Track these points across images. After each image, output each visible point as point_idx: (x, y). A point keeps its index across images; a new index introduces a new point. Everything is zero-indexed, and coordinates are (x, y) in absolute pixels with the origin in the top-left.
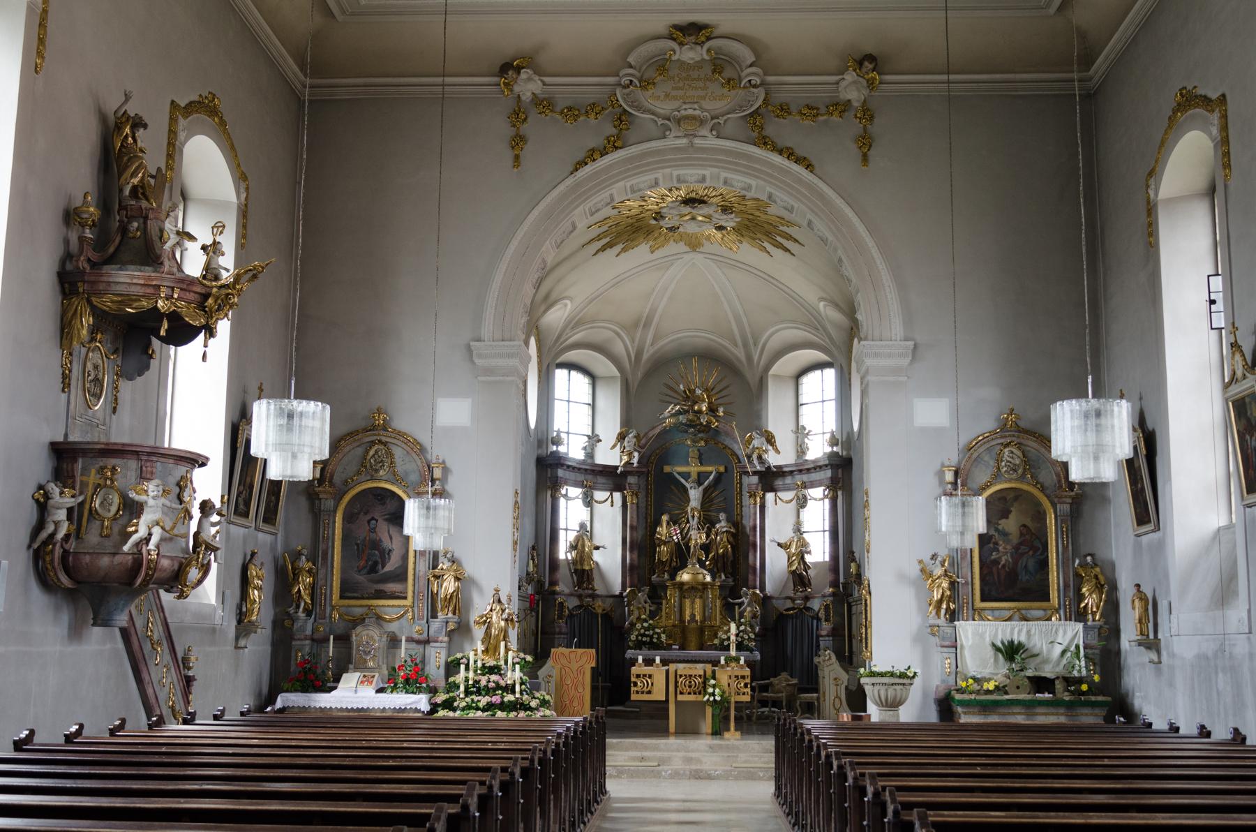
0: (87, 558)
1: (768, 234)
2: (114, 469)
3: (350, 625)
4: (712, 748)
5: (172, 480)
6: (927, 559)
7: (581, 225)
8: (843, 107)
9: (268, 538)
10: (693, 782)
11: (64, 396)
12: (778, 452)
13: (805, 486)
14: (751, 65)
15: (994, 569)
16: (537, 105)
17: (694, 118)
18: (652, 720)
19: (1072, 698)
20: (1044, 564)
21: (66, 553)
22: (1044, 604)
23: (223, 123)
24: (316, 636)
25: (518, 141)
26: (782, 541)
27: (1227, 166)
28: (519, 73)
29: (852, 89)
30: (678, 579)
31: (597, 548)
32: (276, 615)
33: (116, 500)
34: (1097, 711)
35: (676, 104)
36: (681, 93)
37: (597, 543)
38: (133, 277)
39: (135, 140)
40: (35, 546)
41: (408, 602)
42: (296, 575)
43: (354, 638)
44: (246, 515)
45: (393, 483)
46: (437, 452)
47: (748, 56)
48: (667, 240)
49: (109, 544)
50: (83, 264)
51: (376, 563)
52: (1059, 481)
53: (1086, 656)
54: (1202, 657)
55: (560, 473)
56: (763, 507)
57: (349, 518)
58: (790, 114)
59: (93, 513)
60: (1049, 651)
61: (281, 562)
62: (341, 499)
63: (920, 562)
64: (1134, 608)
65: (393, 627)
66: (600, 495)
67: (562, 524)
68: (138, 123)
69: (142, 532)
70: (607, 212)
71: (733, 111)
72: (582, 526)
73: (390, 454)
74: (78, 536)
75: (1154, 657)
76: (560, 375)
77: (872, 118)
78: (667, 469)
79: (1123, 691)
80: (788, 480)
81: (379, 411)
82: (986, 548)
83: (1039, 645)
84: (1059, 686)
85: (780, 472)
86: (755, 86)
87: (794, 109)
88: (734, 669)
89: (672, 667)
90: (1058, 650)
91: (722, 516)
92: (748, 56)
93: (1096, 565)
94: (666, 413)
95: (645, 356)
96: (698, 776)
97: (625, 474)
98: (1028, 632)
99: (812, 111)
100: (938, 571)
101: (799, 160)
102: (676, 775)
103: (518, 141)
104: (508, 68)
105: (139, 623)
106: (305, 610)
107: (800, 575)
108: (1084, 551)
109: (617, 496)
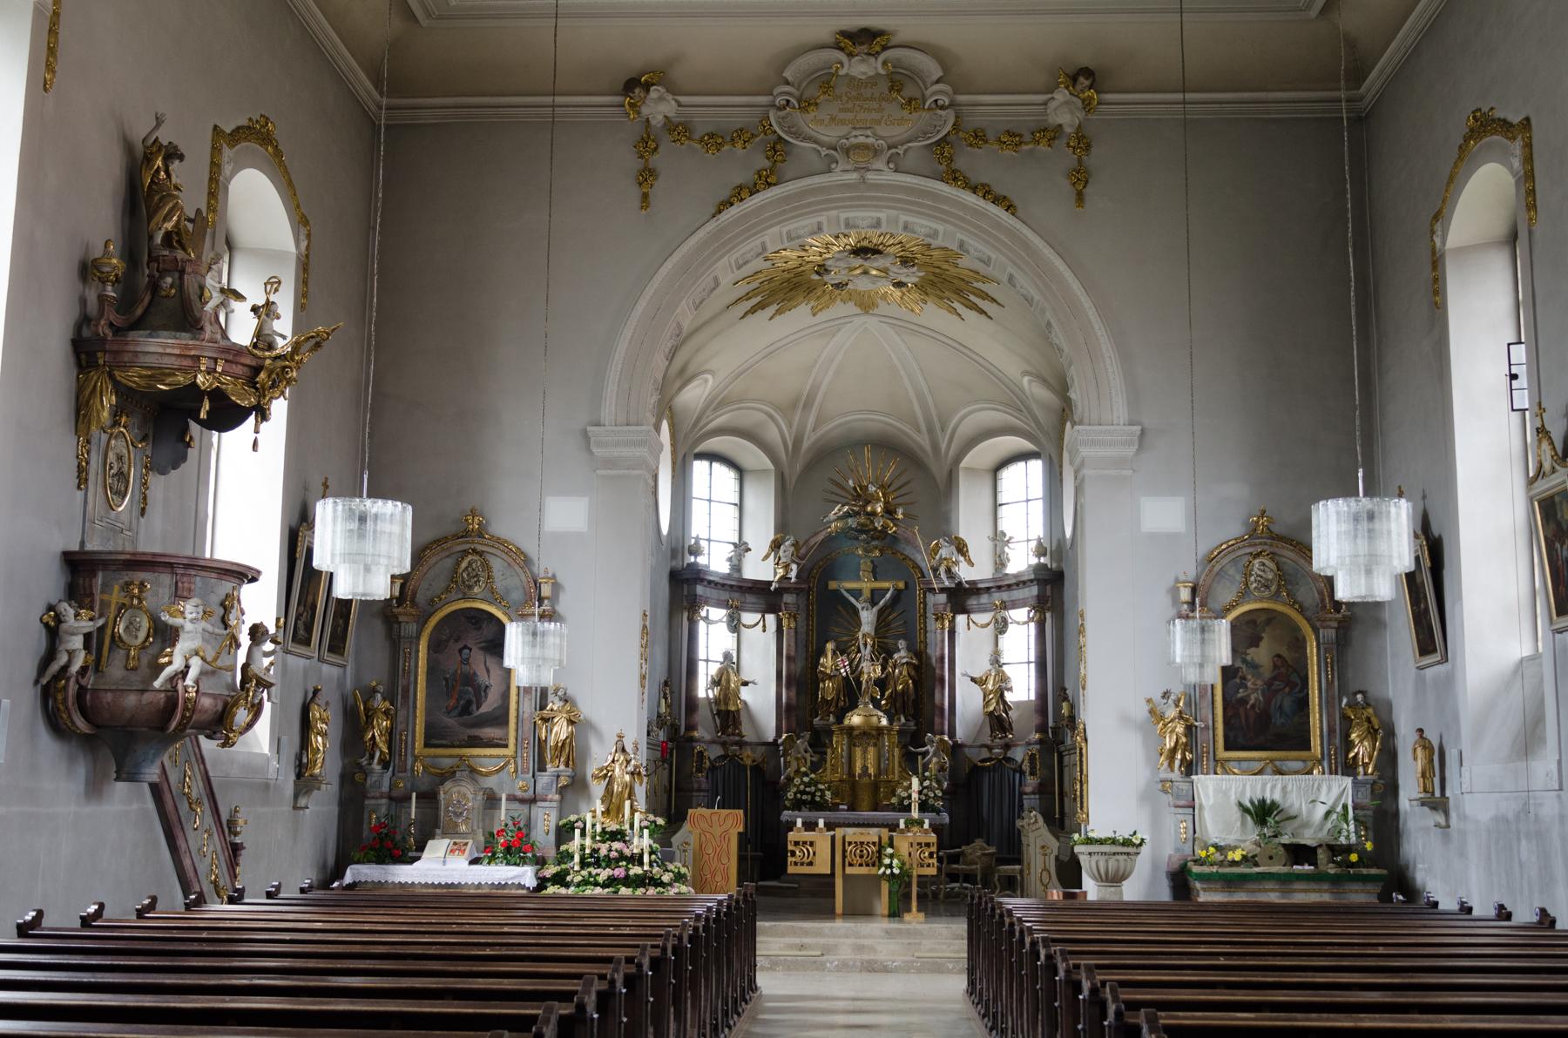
0: (109, 696)
1: (958, 292)
2: (142, 585)
3: (437, 780)
4: (889, 934)
5: (215, 599)
6: (1157, 697)
7: (726, 281)
8: (1052, 133)
9: (335, 671)
10: (865, 975)
11: (80, 494)
12: (971, 564)
13: (1005, 606)
14: (938, 82)
15: (1241, 710)
16: (670, 131)
17: (866, 147)
18: (814, 898)
19: (1338, 871)
20: (1303, 704)
21: (82, 690)
22: (1304, 754)
23: (278, 153)
24: (394, 794)
25: (647, 175)
26: (976, 675)
27: (1532, 207)
28: (648, 91)
29: (1063, 111)
30: (846, 722)
31: (745, 684)
32: (344, 767)
33: (145, 624)
34: (1370, 887)
35: (843, 130)
36: (850, 116)
37: (745, 677)
38: (166, 346)
39: (168, 175)
40: (44, 681)
41: (510, 751)
42: (369, 718)
43: (442, 795)
44: (307, 642)
45: (490, 603)
46: (545, 564)
47: (933, 70)
48: (832, 300)
49: (136, 679)
50: (103, 329)
51: (469, 703)
52: (1323, 600)
53: (1355, 819)
54: (1500, 820)
55: (700, 589)
56: (952, 633)
57: (436, 646)
58: (986, 142)
59: (116, 641)
60: (1310, 813)
61: (350, 701)
62: (426, 622)
63: (1149, 701)
64: (1415, 759)
65: (491, 782)
66: (749, 618)
67: (702, 654)
68: (172, 154)
69: (178, 664)
70: (758, 264)
71: (915, 139)
72: (727, 656)
73: (487, 566)
74: (97, 669)
75: (1441, 819)
76: (700, 468)
77: (1088, 147)
78: (833, 585)
79: (1402, 862)
80: (984, 599)
81: (473, 513)
82: (1231, 683)
83: (1297, 805)
84: (1322, 855)
85: (974, 589)
86: (942, 108)
87: (991, 135)
88: (916, 835)
89: (839, 832)
90: (1321, 811)
91: (902, 644)
92: (933, 70)
93: (1368, 705)
94: (832, 516)
95: (806, 445)
96: (871, 968)
97: (780, 591)
98: (1284, 789)
99: (1013, 138)
100: (1172, 713)
101: (997, 200)
102: (844, 967)
103: (647, 175)
104: (634, 85)
105: (173, 777)
106: (381, 761)
107: (999, 718)
108: (1353, 687)
109: (771, 619)
